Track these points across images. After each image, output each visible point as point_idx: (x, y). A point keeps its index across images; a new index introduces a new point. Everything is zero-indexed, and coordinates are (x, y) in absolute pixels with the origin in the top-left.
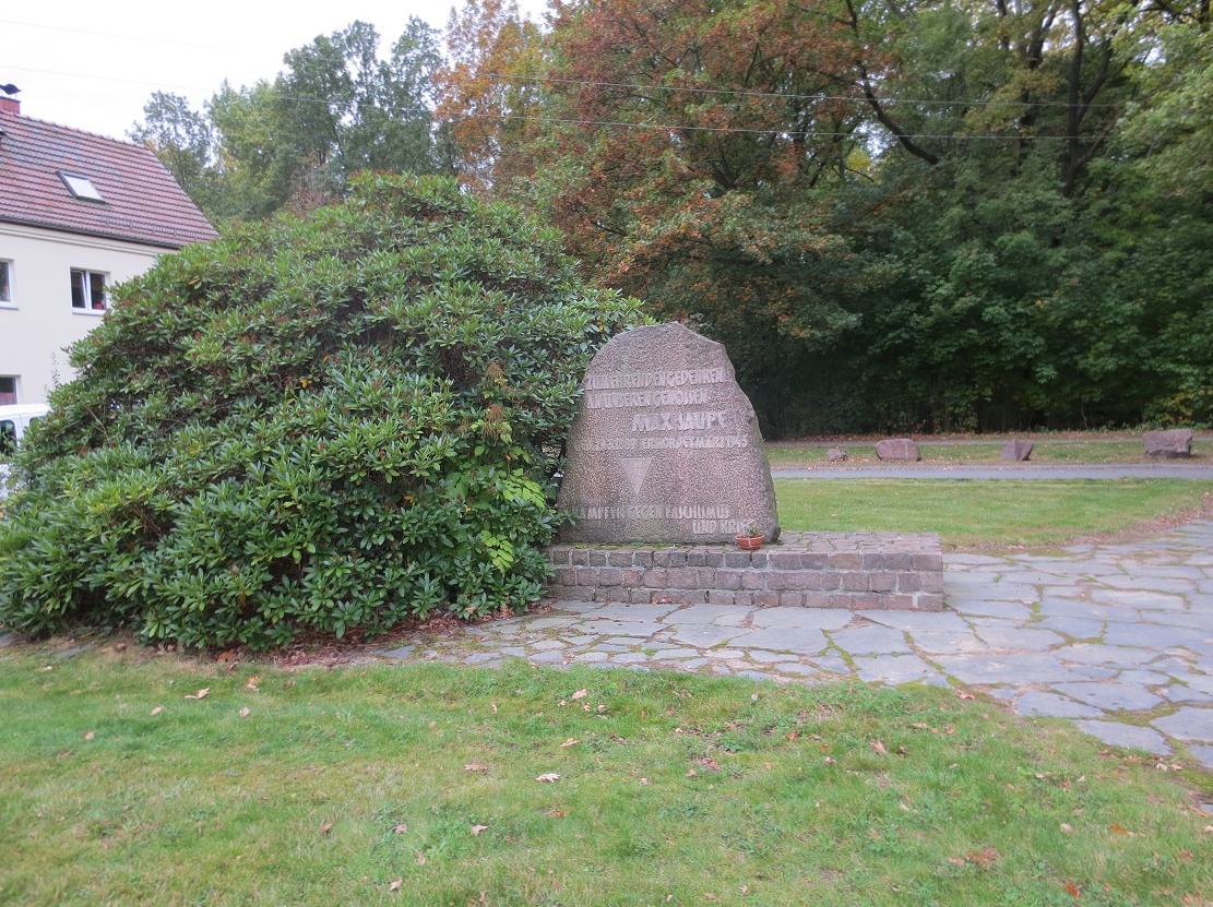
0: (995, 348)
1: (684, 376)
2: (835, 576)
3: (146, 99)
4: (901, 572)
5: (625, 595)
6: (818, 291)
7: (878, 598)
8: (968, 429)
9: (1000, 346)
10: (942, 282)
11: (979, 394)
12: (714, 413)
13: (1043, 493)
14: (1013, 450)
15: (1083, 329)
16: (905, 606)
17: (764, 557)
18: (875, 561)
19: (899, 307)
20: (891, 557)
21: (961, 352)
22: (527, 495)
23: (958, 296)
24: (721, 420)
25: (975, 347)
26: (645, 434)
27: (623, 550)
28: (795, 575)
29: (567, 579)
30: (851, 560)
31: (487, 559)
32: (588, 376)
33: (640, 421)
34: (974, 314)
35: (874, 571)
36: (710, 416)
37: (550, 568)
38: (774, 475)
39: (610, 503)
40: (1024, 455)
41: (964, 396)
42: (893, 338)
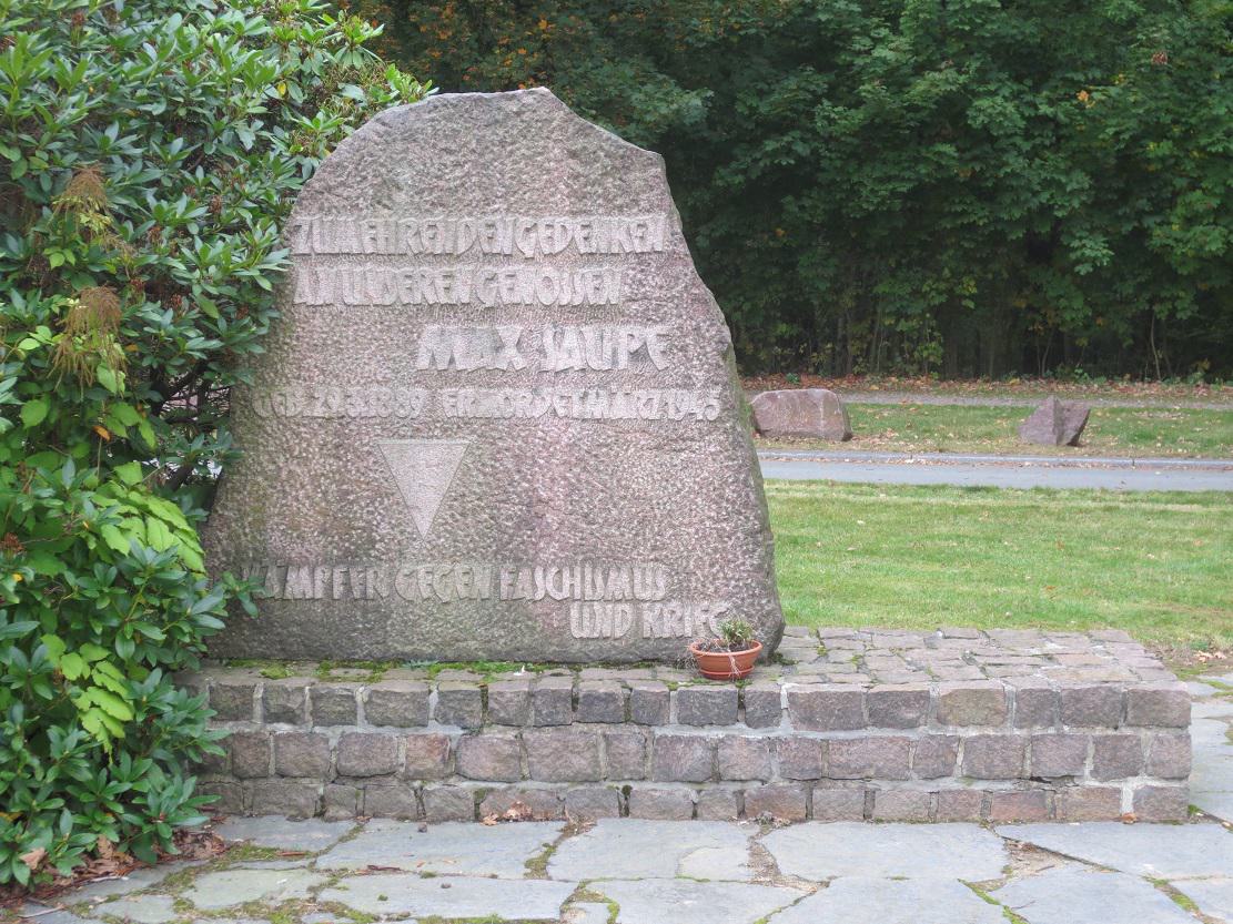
0: (987, 192)
1: (561, 229)
2: (949, 742)
4: (1099, 731)
5: (408, 799)
6: (608, 32)
7: (1042, 794)
9: (1000, 187)
10: (884, 32)
11: (950, 291)
12: (637, 330)
13: (1162, 523)
14: (1050, 421)
15: (1162, 159)
16: (1104, 810)
17: (773, 699)
18: (1043, 707)
19: (792, 83)
20: (1077, 697)
21: (919, 192)
22: (162, 538)
23: (919, 70)
24: (655, 349)
25: (947, 186)
26: (451, 376)
27: (400, 683)
28: (851, 742)
29: (247, 758)
30: (984, 704)
31: (67, 715)
32: (301, 218)
33: (432, 343)
34: (952, 108)
35: (1038, 730)
36: (626, 337)
37: (212, 733)
39: (350, 558)
40: (1071, 434)
41: (917, 293)
42: (775, 153)
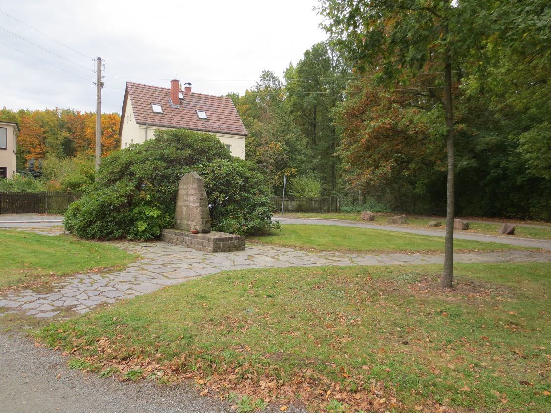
3: (261, 74)
8: (542, 219)
38: (455, 236)
